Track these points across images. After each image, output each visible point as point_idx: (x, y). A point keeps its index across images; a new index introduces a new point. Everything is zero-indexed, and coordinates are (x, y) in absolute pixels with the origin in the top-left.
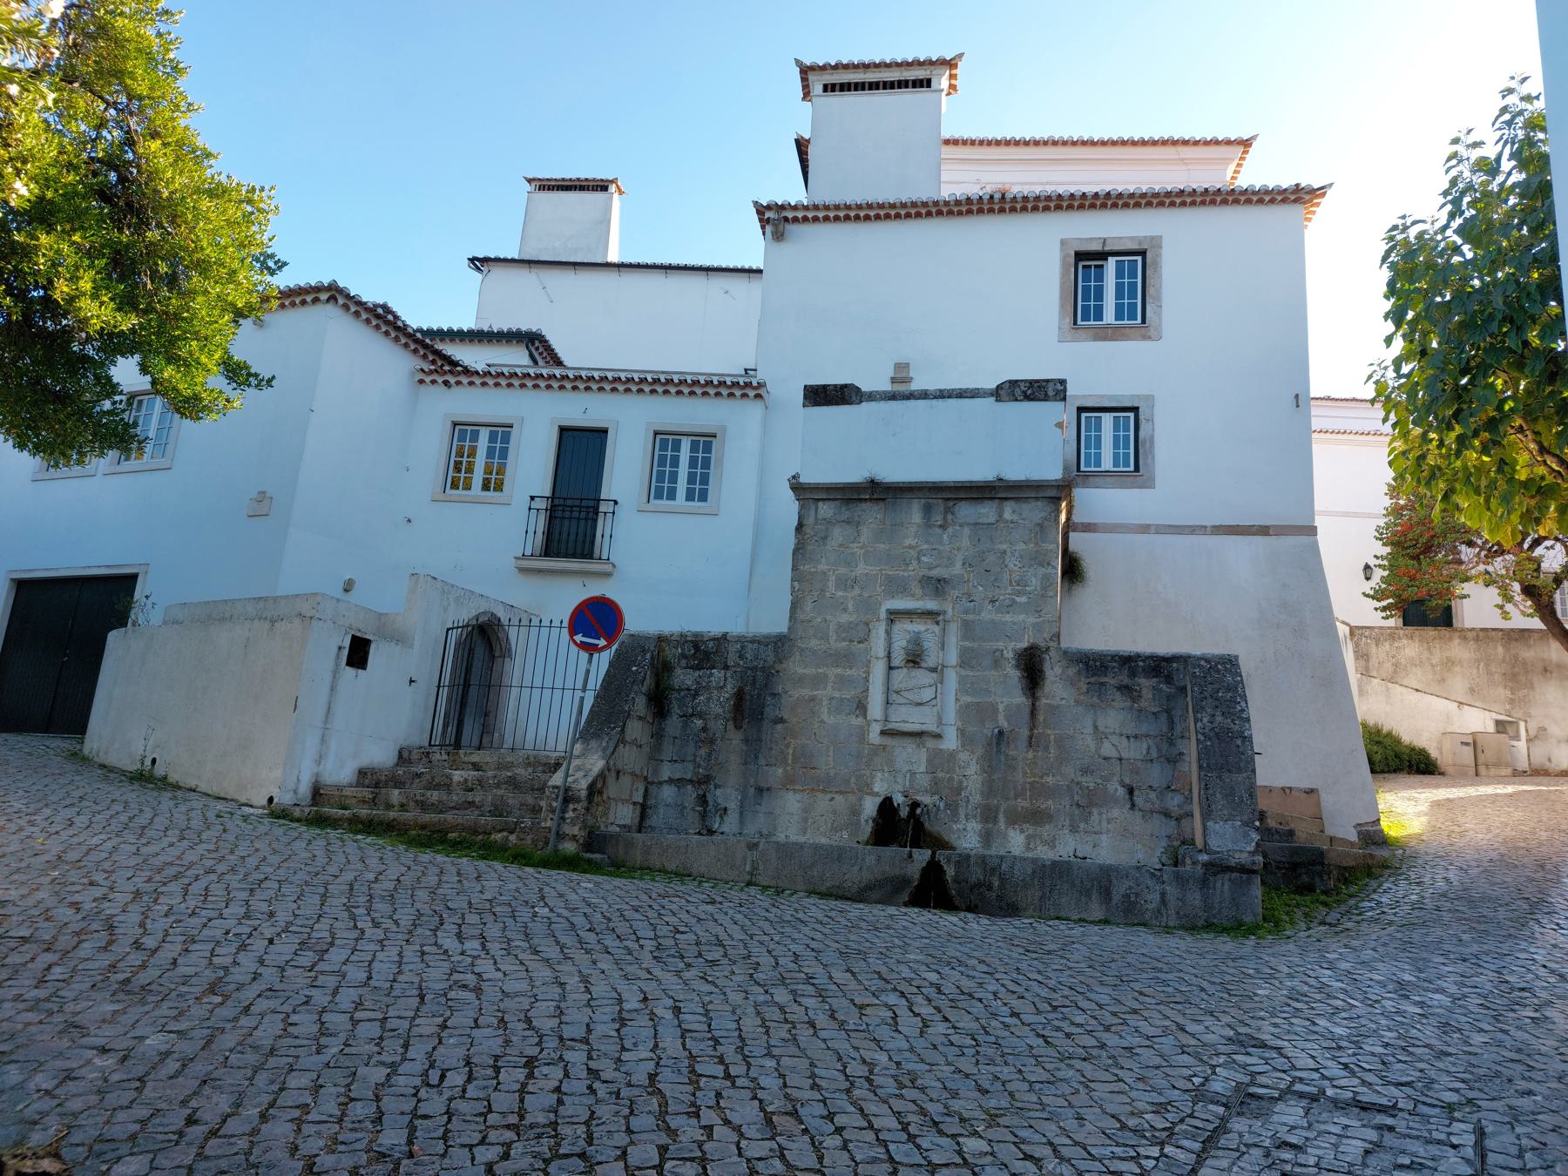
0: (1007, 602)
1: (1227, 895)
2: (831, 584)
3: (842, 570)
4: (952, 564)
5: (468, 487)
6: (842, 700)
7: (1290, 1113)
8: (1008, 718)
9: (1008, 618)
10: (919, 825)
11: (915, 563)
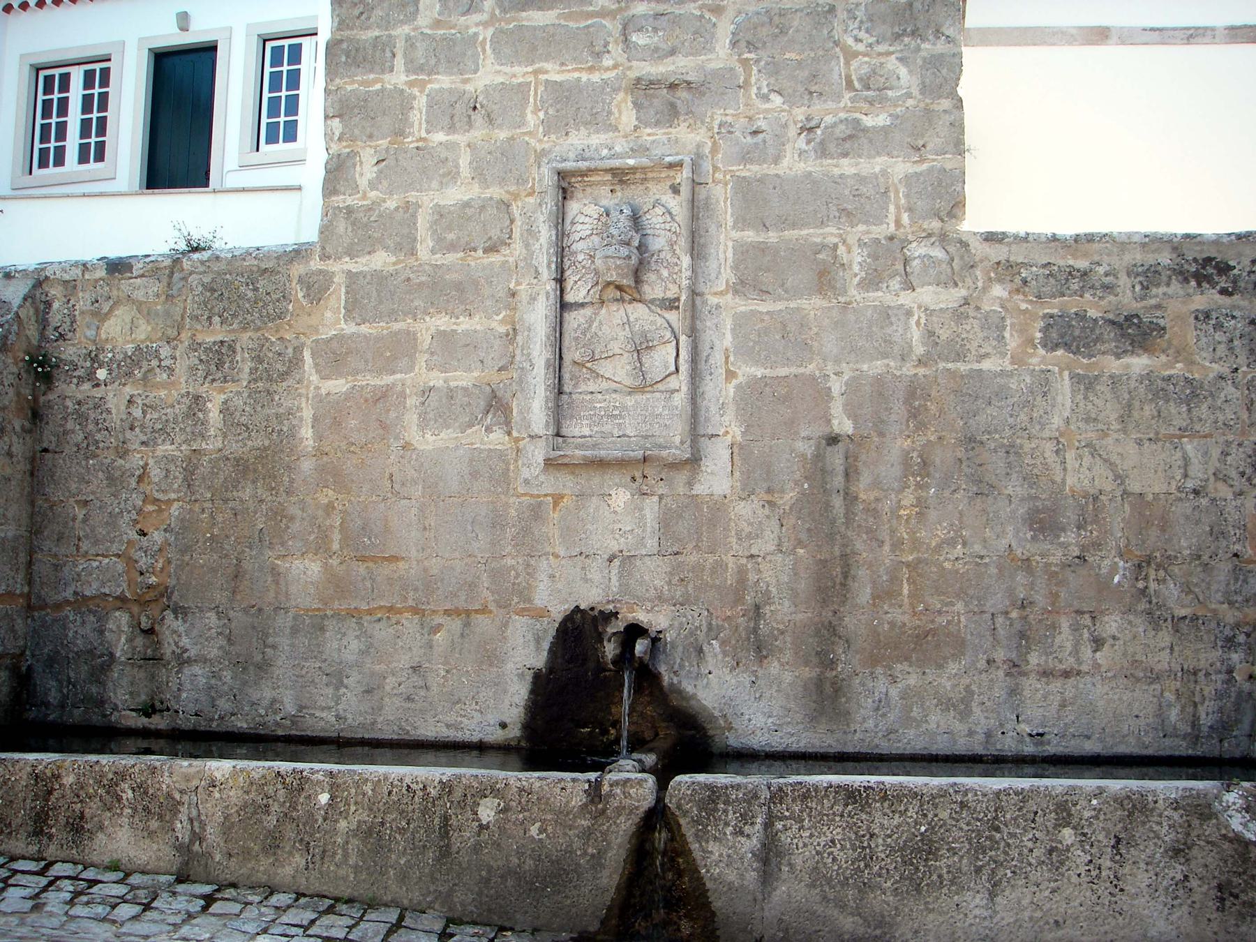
0: (841, 131)
1: (732, 394)
2: (418, 117)
5: (60, 161)
6: (451, 394)
9: (847, 167)
10: (647, 677)
11: (616, 50)
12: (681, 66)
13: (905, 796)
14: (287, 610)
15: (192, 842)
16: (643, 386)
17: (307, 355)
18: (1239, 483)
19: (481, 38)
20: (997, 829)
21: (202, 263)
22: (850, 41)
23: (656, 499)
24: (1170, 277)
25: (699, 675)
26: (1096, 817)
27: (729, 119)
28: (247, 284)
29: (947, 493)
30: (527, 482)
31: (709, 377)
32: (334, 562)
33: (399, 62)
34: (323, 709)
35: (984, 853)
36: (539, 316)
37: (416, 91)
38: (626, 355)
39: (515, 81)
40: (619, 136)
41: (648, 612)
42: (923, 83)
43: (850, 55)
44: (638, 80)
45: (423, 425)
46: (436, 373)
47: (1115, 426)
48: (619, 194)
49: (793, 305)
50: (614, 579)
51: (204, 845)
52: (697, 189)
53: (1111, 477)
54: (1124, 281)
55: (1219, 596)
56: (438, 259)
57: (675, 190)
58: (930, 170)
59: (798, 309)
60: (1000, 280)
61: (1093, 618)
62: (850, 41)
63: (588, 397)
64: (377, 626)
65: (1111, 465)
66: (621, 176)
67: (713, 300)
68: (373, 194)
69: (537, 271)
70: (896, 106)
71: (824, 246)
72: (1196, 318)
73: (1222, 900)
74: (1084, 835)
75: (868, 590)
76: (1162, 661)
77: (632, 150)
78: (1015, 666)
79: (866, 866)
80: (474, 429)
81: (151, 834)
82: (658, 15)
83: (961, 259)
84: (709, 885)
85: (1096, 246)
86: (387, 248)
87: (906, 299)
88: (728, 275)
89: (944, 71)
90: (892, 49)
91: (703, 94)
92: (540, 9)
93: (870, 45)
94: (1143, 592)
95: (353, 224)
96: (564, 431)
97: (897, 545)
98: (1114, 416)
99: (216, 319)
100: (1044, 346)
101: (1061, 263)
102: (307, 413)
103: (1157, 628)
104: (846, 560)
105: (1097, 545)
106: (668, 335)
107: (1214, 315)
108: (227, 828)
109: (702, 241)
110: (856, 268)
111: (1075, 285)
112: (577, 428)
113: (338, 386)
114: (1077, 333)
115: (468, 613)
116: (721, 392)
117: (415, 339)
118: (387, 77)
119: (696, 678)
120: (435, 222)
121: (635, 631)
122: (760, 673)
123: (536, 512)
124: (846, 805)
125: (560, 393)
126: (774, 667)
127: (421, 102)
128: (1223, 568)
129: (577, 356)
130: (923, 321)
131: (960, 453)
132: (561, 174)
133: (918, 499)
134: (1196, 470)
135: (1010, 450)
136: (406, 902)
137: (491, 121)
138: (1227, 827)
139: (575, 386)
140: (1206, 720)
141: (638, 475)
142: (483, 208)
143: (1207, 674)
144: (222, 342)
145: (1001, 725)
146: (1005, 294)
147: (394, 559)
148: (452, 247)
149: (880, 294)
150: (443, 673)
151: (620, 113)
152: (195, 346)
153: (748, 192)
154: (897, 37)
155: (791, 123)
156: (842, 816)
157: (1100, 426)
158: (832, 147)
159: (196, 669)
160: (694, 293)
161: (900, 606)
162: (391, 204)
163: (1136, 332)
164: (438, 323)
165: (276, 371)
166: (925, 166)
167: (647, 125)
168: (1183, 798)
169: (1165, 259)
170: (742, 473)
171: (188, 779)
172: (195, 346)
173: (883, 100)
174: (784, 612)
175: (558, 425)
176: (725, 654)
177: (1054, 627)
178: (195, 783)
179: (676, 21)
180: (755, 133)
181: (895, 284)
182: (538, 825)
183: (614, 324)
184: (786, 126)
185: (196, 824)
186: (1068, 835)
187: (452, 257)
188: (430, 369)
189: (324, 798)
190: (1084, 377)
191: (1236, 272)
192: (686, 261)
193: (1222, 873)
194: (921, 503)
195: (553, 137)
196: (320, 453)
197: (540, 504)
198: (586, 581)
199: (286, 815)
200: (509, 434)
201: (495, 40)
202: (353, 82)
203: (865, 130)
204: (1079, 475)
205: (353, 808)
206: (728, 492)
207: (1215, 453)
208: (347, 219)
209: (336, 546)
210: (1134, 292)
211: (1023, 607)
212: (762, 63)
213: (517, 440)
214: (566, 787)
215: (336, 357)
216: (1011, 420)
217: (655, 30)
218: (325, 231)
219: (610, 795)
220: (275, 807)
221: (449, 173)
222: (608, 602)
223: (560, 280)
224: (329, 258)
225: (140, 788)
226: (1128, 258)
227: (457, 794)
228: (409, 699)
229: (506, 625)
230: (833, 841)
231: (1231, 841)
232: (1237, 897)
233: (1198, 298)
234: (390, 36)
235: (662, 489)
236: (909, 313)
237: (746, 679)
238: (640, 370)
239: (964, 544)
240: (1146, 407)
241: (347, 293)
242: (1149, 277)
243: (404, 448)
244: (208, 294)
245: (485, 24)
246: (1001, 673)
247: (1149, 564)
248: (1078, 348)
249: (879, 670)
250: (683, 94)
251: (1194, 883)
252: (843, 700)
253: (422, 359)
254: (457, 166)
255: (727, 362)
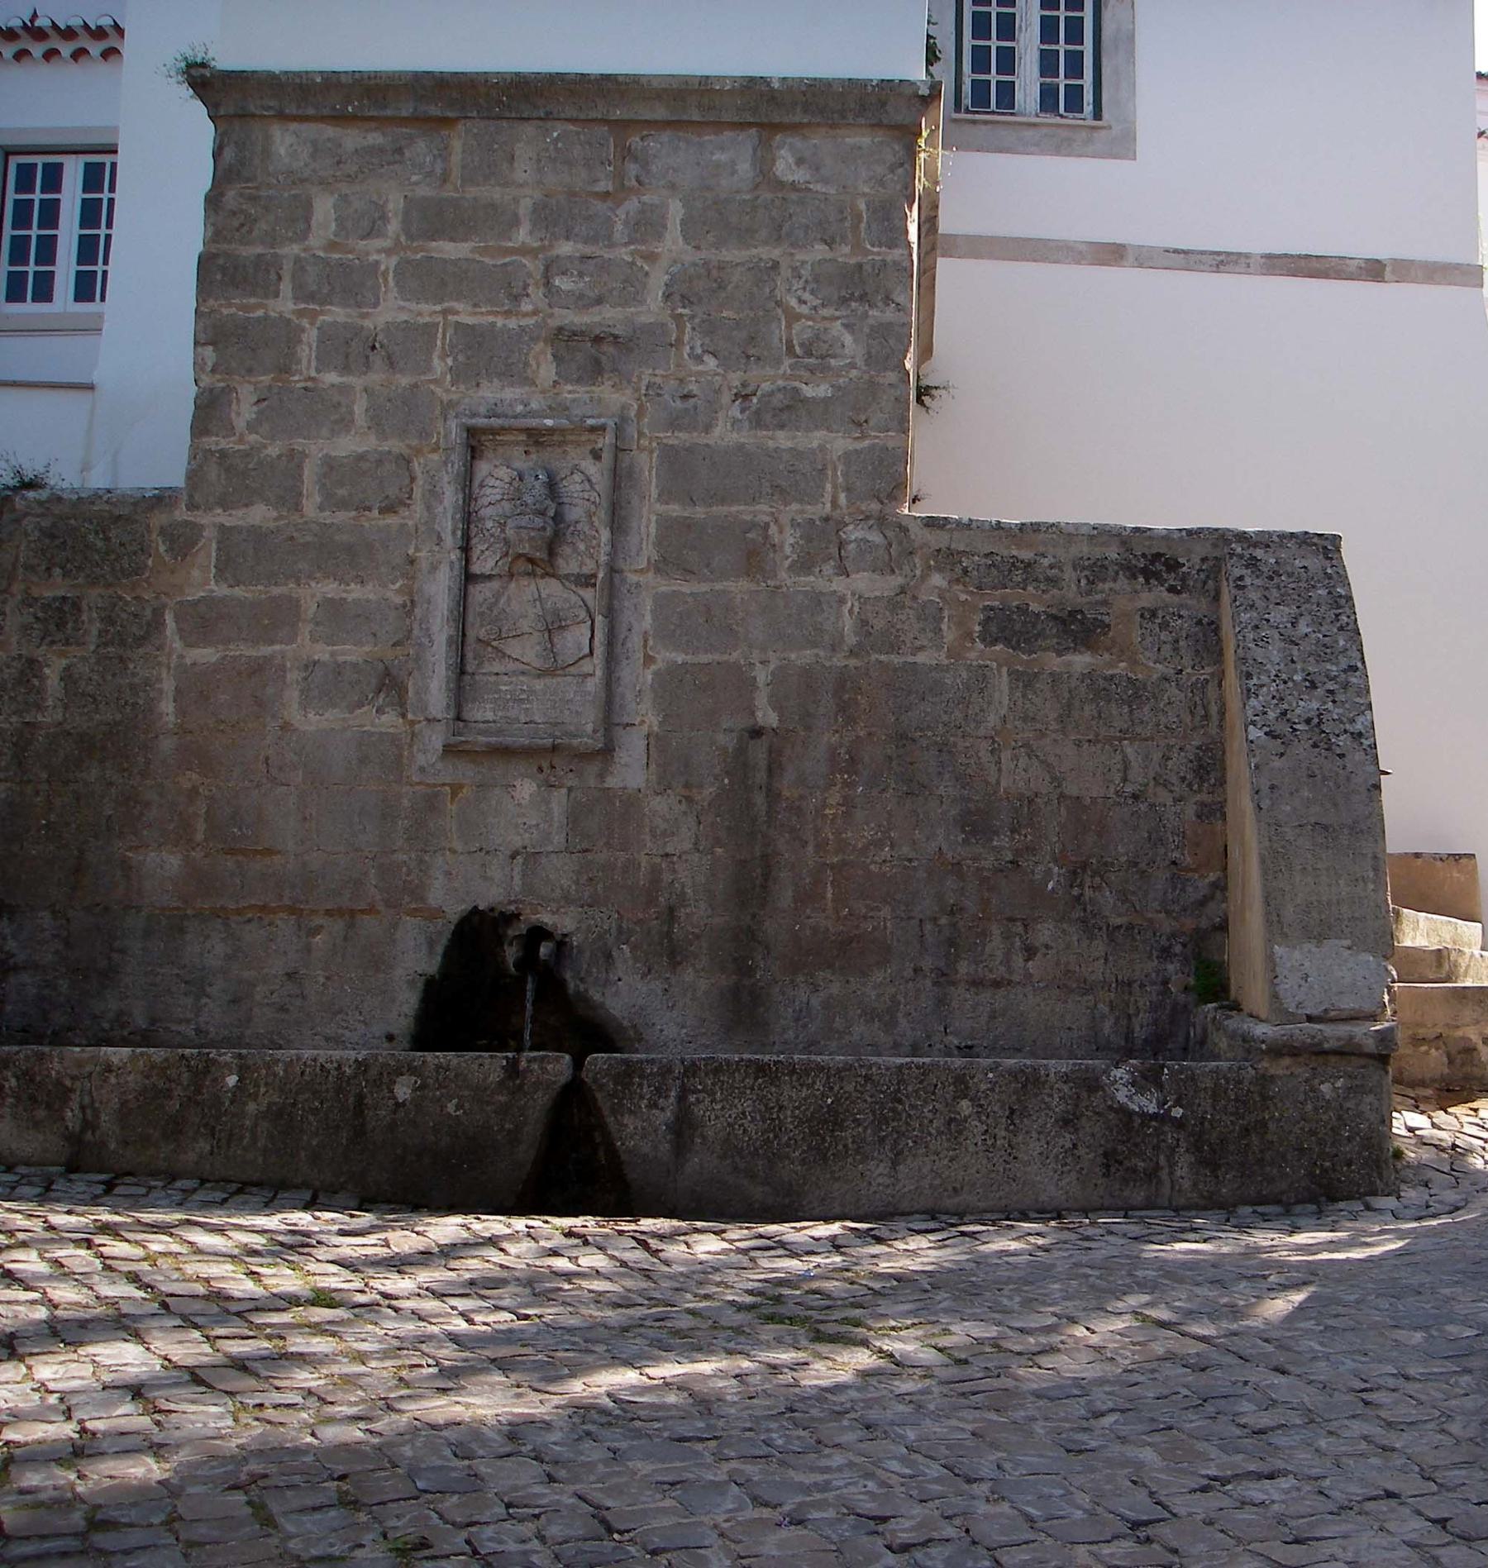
0: (778, 400)
3: (337, 314)
4: (637, 298)
6: (338, 669)
7: (156, 1520)
8: (777, 705)
9: (783, 440)
10: (550, 982)
11: (537, 294)
12: (608, 316)
13: (812, 1069)
14: (139, 909)
15: (83, 1131)
16: (553, 669)
17: (169, 618)
18: (1179, 789)
19: (383, 268)
20: (900, 1101)
21: (40, 503)
22: (793, 302)
23: (564, 791)
24: (1117, 573)
25: (607, 983)
26: (992, 1090)
27: (658, 380)
28: (97, 533)
29: (875, 792)
30: (422, 769)
31: (625, 662)
32: (197, 854)
33: (286, 287)
34: (180, 1022)
35: (887, 1124)
36: (440, 587)
37: (305, 323)
38: (536, 634)
39: (421, 320)
40: (535, 391)
41: (554, 913)
42: (869, 353)
43: (793, 317)
44: (560, 329)
45: (304, 707)
46: (320, 646)
47: (1054, 726)
48: (534, 456)
49: (718, 586)
50: (517, 880)
51: (98, 1133)
52: (620, 455)
53: (1048, 778)
54: (1069, 574)
55: (1156, 905)
56: (326, 517)
57: (596, 455)
58: (872, 447)
59: (724, 591)
60: (939, 570)
61: (1025, 926)
62: (793, 302)
63: (492, 679)
64: (248, 927)
65: (1048, 766)
66: (536, 438)
67: (633, 578)
68: (253, 438)
69: (440, 538)
70: (839, 376)
71: (753, 525)
72: (1142, 616)
73: (1108, 1166)
74: (981, 1106)
75: (790, 893)
76: (1097, 971)
77: (550, 407)
78: (943, 975)
79: (776, 1137)
80: (365, 709)
81: (37, 1125)
82: (585, 258)
83: (900, 546)
84: (624, 1157)
85: (1041, 536)
86: (267, 502)
87: (839, 585)
88: (649, 552)
89: (892, 342)
90: (837, 314)
91: (631, 350)
92: (452, 240)
93: (815, 308)
94: (1078, 898)
95: (227, 470)
96: (466, 715)
97: (821, 846)
98: (1053, 715)
99: (57, 571)
100: (983, 640)
101: (1005, 553)
102: (168, 685)
103: (1091, 938)
104: (768, 863)
105: (1031, 849)
106: (583, 614)
107: (1160, 614)
108: (124, 1114)
109: (623, 513)
110: (788, 550)
111: (1018, 576)
112: (482, 712)
113: (206, 655)
114: (1018, 627)
115: (352, 913)
116: (637, 677)
117: (298, 606)
118: (271, 302)
119: (605, 986)
120: (325, 475)
121: (539, 933)
122: (673, 981)
123: (431, 803)
124: (756, 1079)
125: (463, 672)
126: (689, 975)
127: (311, 335)
128: (1161, 877)
129: (482, 634)
130: (856, 610)
131: (891, 750)
132: (471, 432)
133: (845, 798)
134: (1136, 772)
135: (943, 748)
136: (317, 1183)
137: (391, 364)
138: (1113, 1098)
139: (480, 665)
140: (1140, 1033)
141: (545, 765)
142: (380, 462)
143: (1142, 986)
144: (64, 598)
145: (928, 1037)
146: (944, 584)
147: (269, 852)
148: (343, 504)
149: (812, 578)
150: (322, 980)
151: (538, 365)
152: (29, 601)
153: (675, 461)
154: (844, 301)
155: (725, 389)
156: (752, 1089)
157: (1038, 726)
158: (767, 417)
159: (25, 977)
160: (613, 570)
161: (824, 911)
162: (273, 451)
163: (1080, 629)
164: (325, 589)
165: (130, 635)
166: (867, 443)
167: (568, 381)
168: (1073, 1071)
169: (1113, 554)
170: (658, 765)
171: (80, 1064)
172: (29, 601)
173: (825, 368)
174: (700, 915)
175: (459, 707)
176: (636, 959)
177: (984, 934)
178: (88, 1069)
179: (605, 266)
180: (685, 397)
181: (829, 568)
182: (455, 1101)
183: (523, 599)
184: (718, 391)
185: (89, 1111)
186: (965, 1106)
187: (343, 516)
188: (314, 640)
189: (232, 1080)
190: (1023, 673)
191: (1184, 569)
192: (605, 535)
193: (1107, 1141)
194: (848, 803)
195: (462, 387)
196: (182, 730)
197: (436, 795)
198: (485, 878)
199: (189, 1098)
200: (404, 716)
201: (399, 272)
202: (230, 305)
203: (805, 401)
204: (1015, 776)
205: (263, 1090)
206: (643, 785)
207: (1157, 756)
208: (220, 464)
209: (199, 837)
210: (1079, 586)
211: (952, 913)
212: (697, 320)
213: (412, 723)
214: (488, 1066)
215: (204, 622)
216: (945, 718)
217: (581, 275)
218: (193, 476)
219: (528, 1070)
220: (178, 1091)
221: (343, 420)
222: (510, 903)
223: (466, 549)
224: (198, 508)
225: (26, 1077)
226: (1074, 551)
227: (373, 1072)
228: (283, 1009)
229: (395, 926)
230: (743, 1113)
231: (1116, 1111)
232: (1121, 1163)
233: (1145, 595)
234: (276, 255)
235: (571, 781)
236: (842, 601)
237: (657, 986)
238: (551, 650)
239: (892, 846)
240: (1086, 708)
241: (219, 549)
242: (1096, 571)
243: (282, 728)
244: (47, 541)
245: (388, 252)
246: (928, 983)
247: (1084, 868)
248: (1018, 642)
249: (800, 978)
250: (609, 349)
251: (1081, 1151)
252: (762, 1009)
253: (305, 630)
254: (351, 413)
255: (645, 646)
